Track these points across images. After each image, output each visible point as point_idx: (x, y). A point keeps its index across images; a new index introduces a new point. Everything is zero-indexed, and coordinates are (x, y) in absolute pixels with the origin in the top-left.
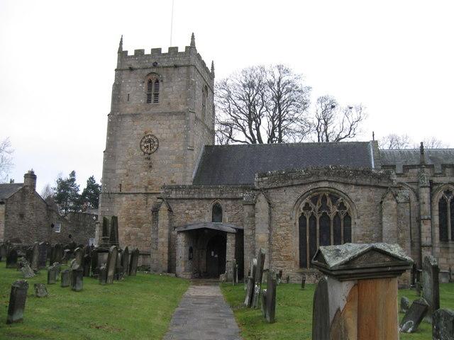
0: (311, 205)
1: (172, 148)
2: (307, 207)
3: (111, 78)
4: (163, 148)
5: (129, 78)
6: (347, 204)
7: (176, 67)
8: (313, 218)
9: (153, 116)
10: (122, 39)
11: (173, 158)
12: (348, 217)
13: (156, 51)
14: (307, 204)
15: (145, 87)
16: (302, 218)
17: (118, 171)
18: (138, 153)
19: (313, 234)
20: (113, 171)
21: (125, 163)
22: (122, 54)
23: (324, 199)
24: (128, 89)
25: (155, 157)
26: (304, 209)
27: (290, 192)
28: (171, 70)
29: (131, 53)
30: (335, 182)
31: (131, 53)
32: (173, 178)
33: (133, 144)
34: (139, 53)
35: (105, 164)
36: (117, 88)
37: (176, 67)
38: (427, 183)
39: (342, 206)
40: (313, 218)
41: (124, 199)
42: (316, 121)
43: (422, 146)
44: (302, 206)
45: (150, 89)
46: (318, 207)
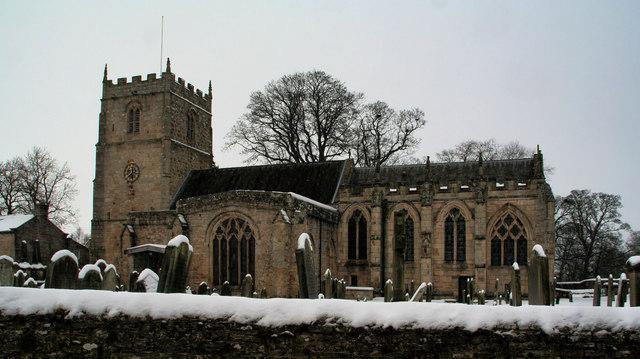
0: (223, 228)
1: (151, 176)
2: (219, 231)
3: (97, 109)
4: (144, 175)
5: (113, 108)
6: (251, 227)
7: (153, 94)
8: (224, 240)
9: (134, 144)
10: (168, 62)
11: (152, 185)
12: (252, 239)
13: (137, 79)
14: (219, 228)
15: (125, 116)
16: (215, 240)
17: (107, 200)
18: (123, 182)
19: (224, 256)
20: (102, 200)
21: (112, 192)
22: (107, 83)
23: (233, 222)
24: (113, 119)
25: (138, 186)
26: (217, 232)
27: (204, 215)
28: (149, 99)
29: (115, 82)
30: (511, 197)
31: (115, 82)
32: (153, 205)
33: (119, 173)
34: (122, 81)
35: (94, 194)
36: (103, 117)
37: (153, 94)
38: (377, 201)
39: (248, 229)
40: (224, 240)
41: (112, 226)
42: (395, 140)
43: (428, 161)
44: (215, 229)
45: (131, 119)
46: (228, 230)
